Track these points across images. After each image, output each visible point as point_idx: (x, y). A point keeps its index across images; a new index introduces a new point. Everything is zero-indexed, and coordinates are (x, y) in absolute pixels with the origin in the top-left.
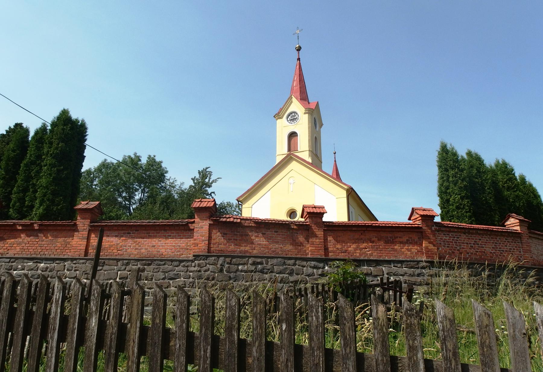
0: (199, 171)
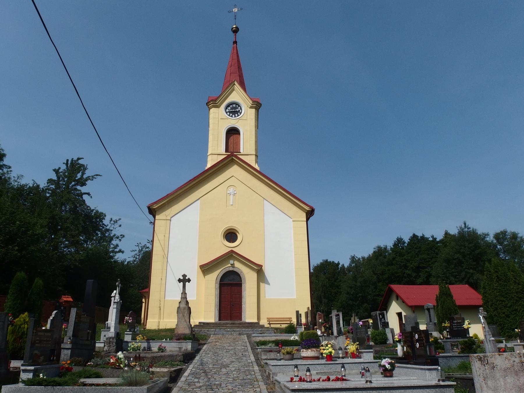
0: (73, 159)
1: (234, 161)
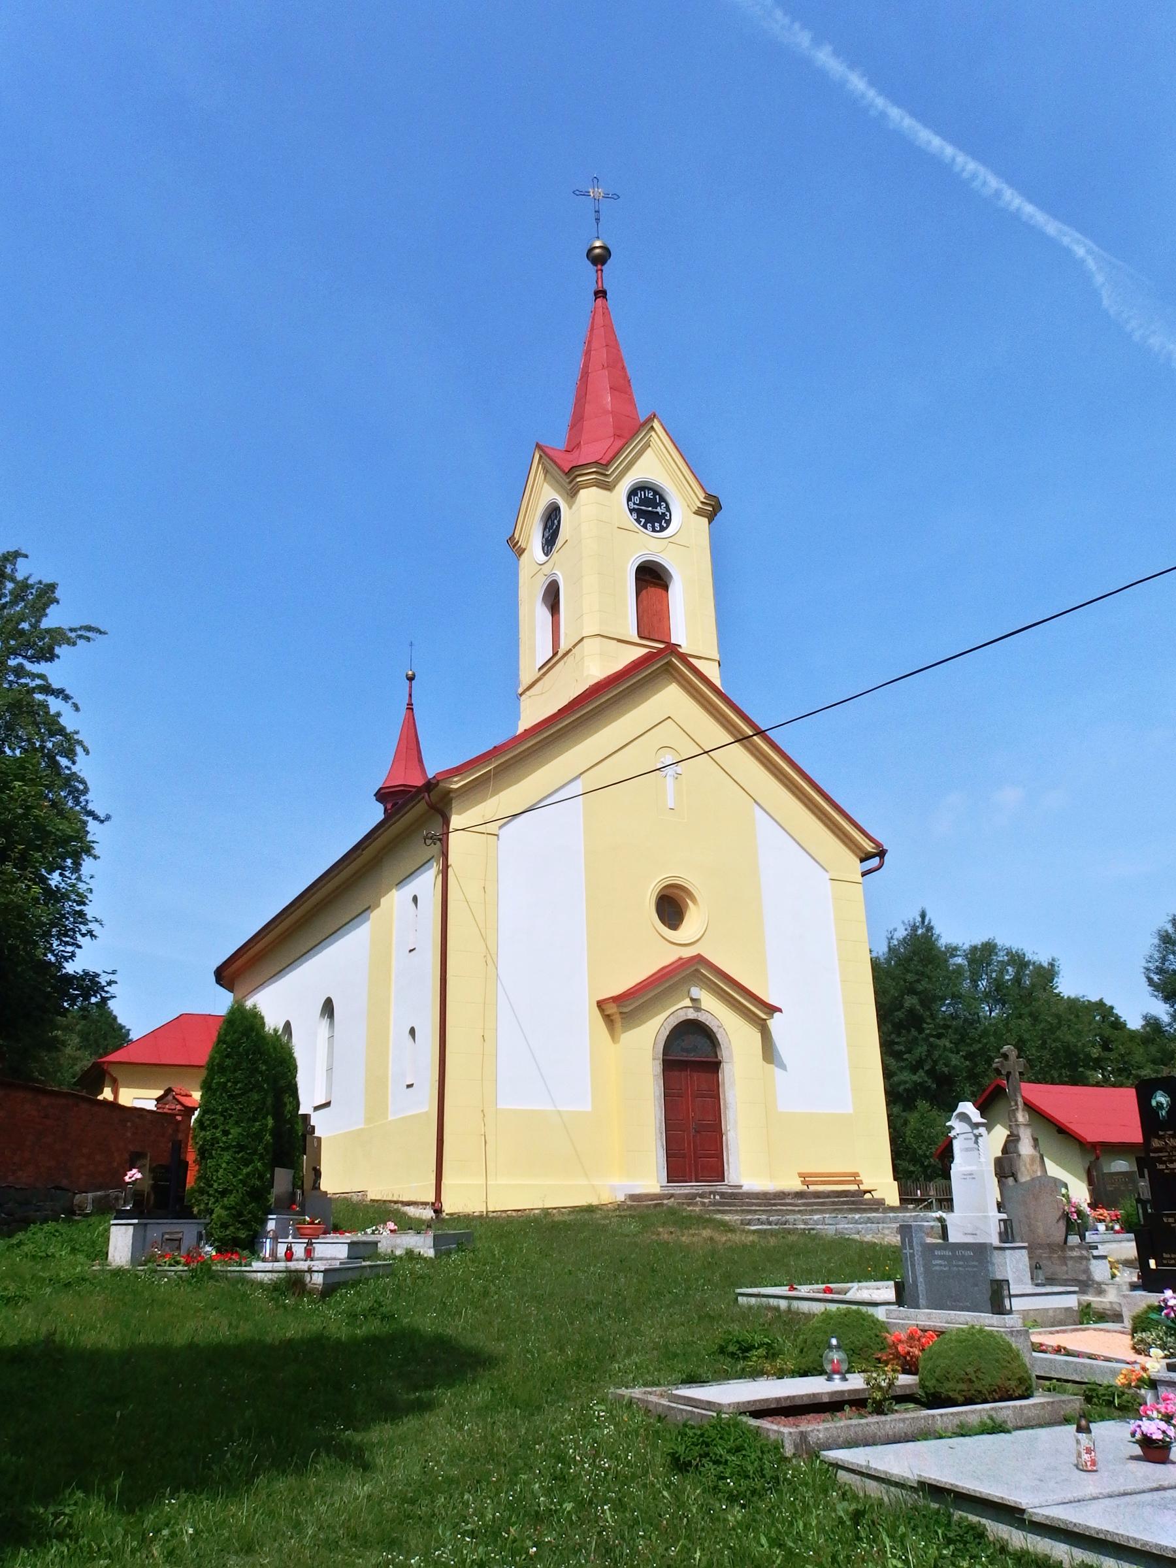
1: (671, 670)
